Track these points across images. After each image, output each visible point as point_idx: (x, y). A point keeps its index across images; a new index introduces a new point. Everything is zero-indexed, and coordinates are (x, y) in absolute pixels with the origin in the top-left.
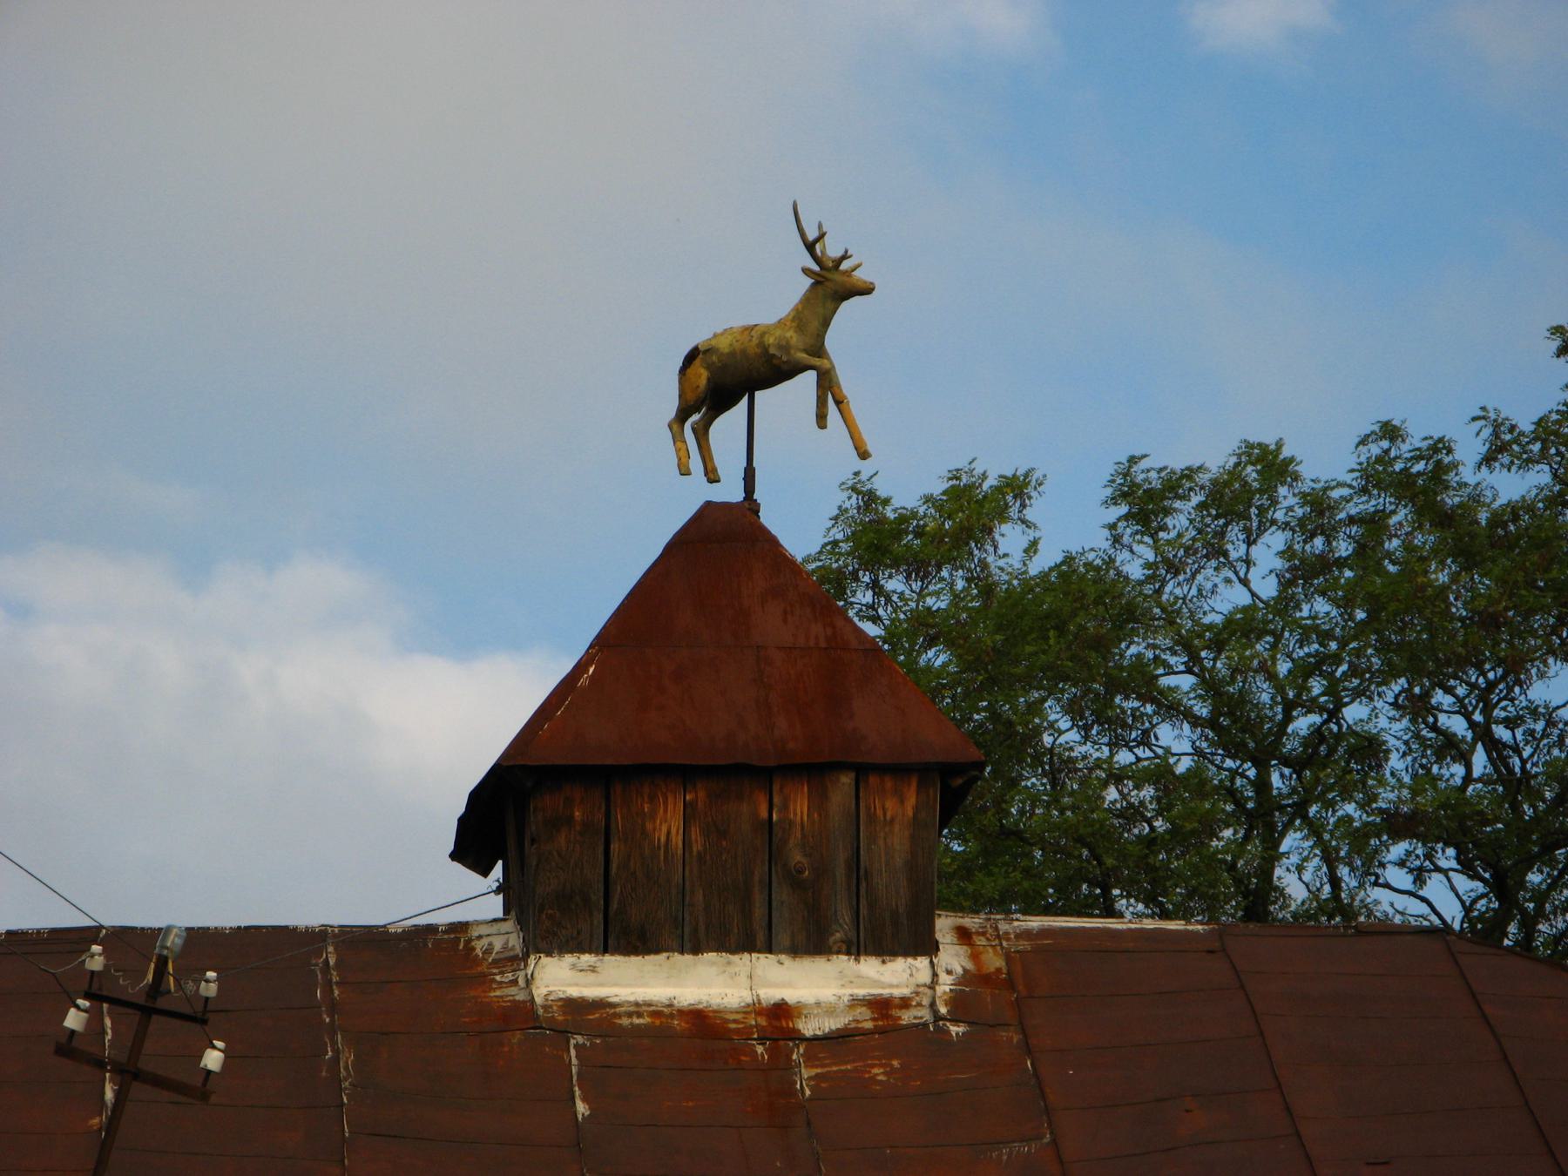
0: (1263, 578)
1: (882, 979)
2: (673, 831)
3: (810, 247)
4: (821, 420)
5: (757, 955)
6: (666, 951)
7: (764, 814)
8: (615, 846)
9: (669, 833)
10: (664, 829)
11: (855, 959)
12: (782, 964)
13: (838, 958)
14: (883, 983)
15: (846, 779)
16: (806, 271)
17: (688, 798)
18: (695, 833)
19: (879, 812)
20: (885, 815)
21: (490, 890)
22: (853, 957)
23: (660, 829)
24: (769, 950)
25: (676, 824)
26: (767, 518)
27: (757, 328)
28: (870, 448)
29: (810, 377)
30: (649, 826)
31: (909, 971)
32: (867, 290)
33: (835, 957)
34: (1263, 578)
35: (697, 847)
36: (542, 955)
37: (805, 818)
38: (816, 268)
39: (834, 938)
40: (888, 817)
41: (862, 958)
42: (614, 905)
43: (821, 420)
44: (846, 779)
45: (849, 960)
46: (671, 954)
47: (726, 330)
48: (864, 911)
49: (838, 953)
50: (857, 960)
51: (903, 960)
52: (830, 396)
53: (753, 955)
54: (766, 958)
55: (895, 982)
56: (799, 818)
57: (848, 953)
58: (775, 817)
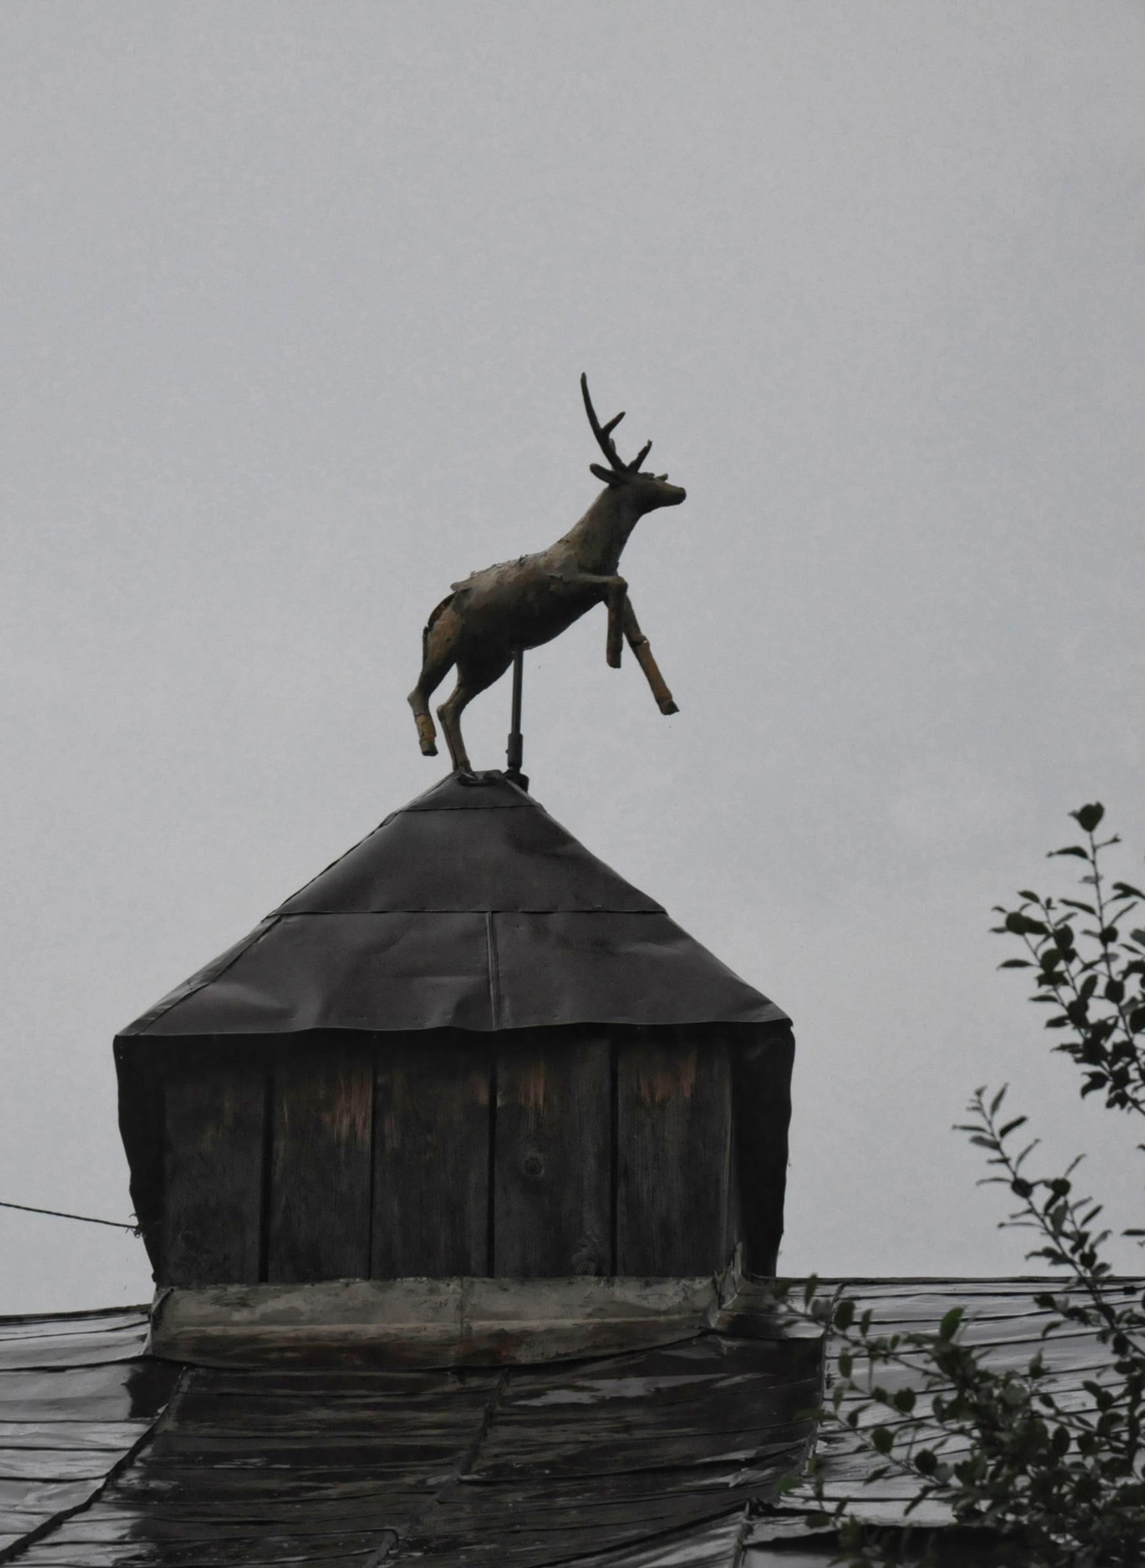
0: (1037, 1141)
1: (645, 1304)
2: (359, 1122)
3: (603, 436)
4: (614, 660)
5: (469, 1278)
6: (344, 1277)
7: (483, 1098)
8: (281, 1145)
9: (353, 1125)
10: (346, 1121)
11: (608, 1281)
12: (506, 1290)
13: (583, 1279)
14: (645, 1309)
15: (598, 1052)
16: (596, 470)
17: (380, 1080)
18: (390, 1126)
19: (645, 1092)
20: (652, 1096)
21: (863, 1478)
22: (605, 1278)
23: (341, 1122)
24: (490, 1270)
25: (362, 1116)
26: (535, 792)
27: (662, 915)
28: (676, 700)
29: (598, 616)
30: (326, 1118)
31: (682, 1294)
32: (676, 497)
33: (579, 1278)
34: (1037, 1141)
35: (392, 1142)
36: (175, 1288)
37: (541, 1102)
38: (607, 466)
39: (579, 1254)
40: (658, 1098)
41: (617, 1279)
42: (277, 1221)
43: (614, 660)
44: (598, 1052)
45: (598, 1283)
46: (351, 1280)
47: (495, 565)
48: (622, 1220)
49: (585, 1273)
50: (611, 1284)
51: (675, 1282)
52: (624, 638)
53: (465, 1279)
54: (484, 1282)
55: (663, 1307)
56: (531, 1104)
57: (599, 1273)
58: (499, 1103)
